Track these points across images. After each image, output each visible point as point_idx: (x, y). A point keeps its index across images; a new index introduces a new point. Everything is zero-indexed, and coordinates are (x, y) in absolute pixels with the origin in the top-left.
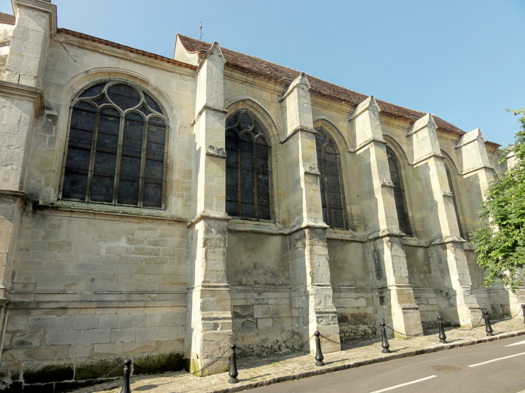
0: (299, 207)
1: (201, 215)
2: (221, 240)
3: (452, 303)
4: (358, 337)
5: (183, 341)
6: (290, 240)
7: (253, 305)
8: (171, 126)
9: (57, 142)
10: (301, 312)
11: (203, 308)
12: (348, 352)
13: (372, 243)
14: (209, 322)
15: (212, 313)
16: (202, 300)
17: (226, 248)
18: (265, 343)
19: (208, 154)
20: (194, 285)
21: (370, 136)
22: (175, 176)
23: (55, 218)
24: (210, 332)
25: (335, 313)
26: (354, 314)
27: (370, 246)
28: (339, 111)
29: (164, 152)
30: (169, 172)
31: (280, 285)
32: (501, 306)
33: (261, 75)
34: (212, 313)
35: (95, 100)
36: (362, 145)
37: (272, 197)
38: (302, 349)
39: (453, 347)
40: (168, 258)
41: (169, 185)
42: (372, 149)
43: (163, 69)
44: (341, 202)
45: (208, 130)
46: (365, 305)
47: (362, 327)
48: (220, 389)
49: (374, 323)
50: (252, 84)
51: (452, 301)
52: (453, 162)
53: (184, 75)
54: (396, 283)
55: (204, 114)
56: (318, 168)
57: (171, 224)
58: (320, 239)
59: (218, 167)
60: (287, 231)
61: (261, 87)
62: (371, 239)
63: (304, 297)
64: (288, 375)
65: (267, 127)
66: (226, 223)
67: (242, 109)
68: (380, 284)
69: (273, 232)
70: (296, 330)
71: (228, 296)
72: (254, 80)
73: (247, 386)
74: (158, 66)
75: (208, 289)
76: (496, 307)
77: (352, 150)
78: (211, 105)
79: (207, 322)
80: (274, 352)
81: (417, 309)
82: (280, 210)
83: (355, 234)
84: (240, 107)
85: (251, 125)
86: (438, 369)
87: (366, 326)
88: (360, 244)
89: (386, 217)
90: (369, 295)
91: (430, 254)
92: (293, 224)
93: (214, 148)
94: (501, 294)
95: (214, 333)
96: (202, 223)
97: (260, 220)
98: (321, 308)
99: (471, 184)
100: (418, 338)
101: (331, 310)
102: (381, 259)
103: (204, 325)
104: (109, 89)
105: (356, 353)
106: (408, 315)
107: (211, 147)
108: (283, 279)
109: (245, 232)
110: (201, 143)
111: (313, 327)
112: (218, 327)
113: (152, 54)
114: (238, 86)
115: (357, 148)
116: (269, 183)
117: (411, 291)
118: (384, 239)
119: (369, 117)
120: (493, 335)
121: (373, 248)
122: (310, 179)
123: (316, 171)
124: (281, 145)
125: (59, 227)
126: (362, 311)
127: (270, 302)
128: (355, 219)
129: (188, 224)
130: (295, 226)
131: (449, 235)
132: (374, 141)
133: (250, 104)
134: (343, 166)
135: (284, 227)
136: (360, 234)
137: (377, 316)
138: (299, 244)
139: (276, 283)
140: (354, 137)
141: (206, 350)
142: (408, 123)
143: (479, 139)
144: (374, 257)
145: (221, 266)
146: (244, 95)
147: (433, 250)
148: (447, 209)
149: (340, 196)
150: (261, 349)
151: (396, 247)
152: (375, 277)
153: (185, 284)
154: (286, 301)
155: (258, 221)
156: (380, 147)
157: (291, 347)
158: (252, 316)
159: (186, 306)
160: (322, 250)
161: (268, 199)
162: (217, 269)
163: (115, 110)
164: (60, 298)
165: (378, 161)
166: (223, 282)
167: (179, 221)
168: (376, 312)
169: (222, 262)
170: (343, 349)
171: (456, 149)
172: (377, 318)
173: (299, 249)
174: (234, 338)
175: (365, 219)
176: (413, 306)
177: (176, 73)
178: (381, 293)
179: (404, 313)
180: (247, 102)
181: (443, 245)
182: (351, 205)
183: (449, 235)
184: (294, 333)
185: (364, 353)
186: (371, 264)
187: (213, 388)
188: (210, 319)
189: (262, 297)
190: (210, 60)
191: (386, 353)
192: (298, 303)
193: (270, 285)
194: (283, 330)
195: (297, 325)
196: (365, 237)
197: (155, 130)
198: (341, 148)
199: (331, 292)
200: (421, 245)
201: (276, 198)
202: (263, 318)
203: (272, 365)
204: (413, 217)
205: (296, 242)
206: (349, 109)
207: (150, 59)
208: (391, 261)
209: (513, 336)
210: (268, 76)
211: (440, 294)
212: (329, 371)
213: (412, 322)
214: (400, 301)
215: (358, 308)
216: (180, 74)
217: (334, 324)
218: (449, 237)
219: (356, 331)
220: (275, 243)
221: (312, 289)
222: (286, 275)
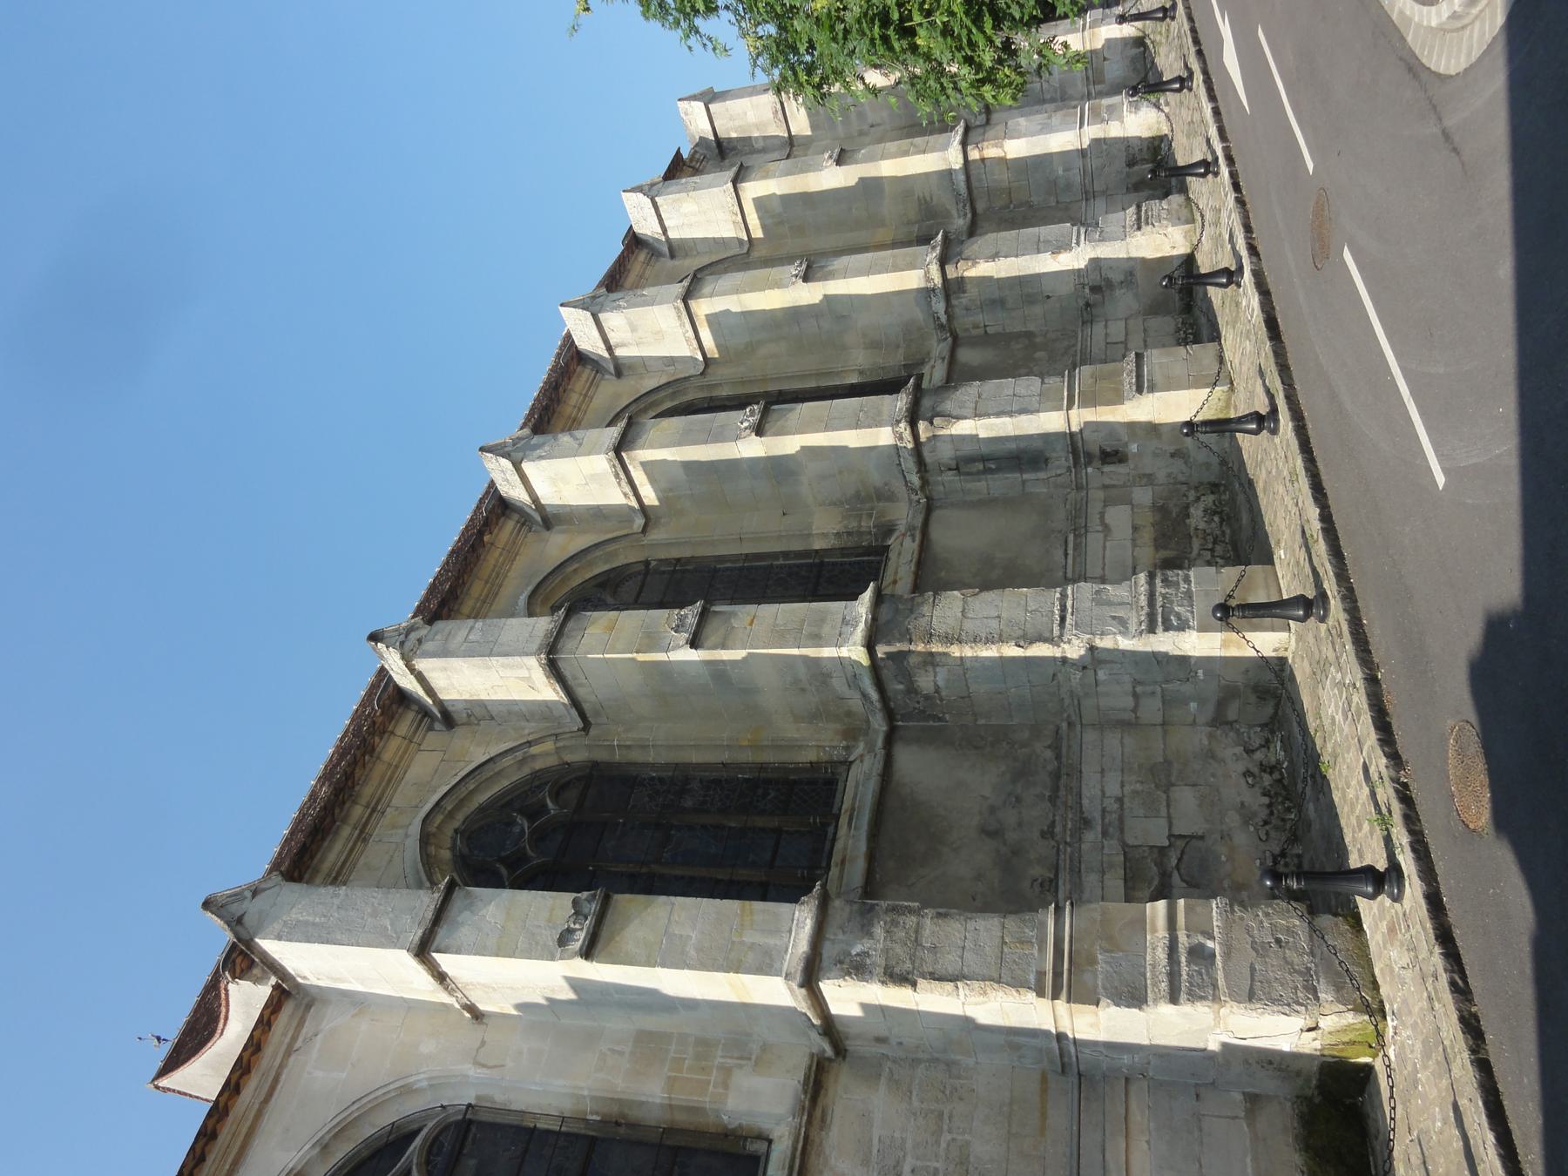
0: (802, 672)
1: (801, 986)
2: (895, 923)
3: (1122, 278)
4: (1228, 531)
5: (1254, 1101)
6: (907, 717)
7: (1124, 845)
8: (467, 1097)
10: (1149, 689)
11: (1133, 998)
12: (1278, 542)
13: (934, 478)
14: (1185, 977)
15: (1153, 966)
16: (1104, 1002)
17: (925, 905)
18: (1255, 814)
19: (588, 953)
20: (1047, 1033)
21: (601, 463)
22: (651, 1092)
24: (1220, 976)
25: (1151, 577)
26: (1155, 540)
27: (946, 482)
28: (511, 553)
29: (559, 1133)
30: (635, 1114)
31: (1058, 757)
32: (1131, 163)
33: (349, 776)
34: (1153, 966)
36: (628, 489)
37: (762, 767)
38: (1272, 686)
39: (1253, 250)
40: (946, 1137)
41: (682, 1119)
42: (639, 456)
43: (259, 1114)
44: (798, 566)
45: (504, 949)
46: (1128, 508)
47: (1197, 518)
48: (1429, 925)
49: (1184, 488)
50: (374, 810)
51: (1116, 277)
52: (711, 265)
53: (294, 1039)
54: (1060, 409)
55: (444, 961)
56: (682, 607)
57: (823, 1120)
58: (912, 611)
59: (636, 921)
60: (879, 724)
61: (393, 777)
62: (922, 478)
63: (1102, 675)
64: (1364, 698)
65: (526, 771)
66: (837, 903)
67: (453, 848)
68: (1061, 460)
69: (878, 766)
70: (1210, 709)
71: (1094, 910)
72: (364, 801)
73: (1411, 832)
74: (244, 1131)
75: (1069, 982)
76: (1134, 179)
77: (639, 522)
78: (416, 935)
79: (1184, 985)
80: (1285, 787)
81: (1139, 357)
82: (812, 744)
83: (902, 528)
84: (446, 854)
85: (512, 823)
86: (1322, 252)
87: (1192, 510)
88: (937, 514)
89: (857, 427)
90: (1097, 495)
91: (975, 332)
92: (856, 703)
93: (570, 931)
94: (1096, 163)
95: (1225, 963)
96: (827, 987)
97: (835, 811)
98: (1136, 619)
99: (781, 223)
100: (1228, 355)
101: (1143, 588)
102: (985, 450)
103: (1194, 997)
105: (1281, 513)
106: (1158, 378)
107: (564, 939)
108: (1038, 747)
109: (871, 857)
110: (547, 977)
111: (1200, 644)
112: (1202, 946)
113: (192, 1148)
114: (374, 853)
115: (634, 503)
116: (715, 775)
117: (1086, 370)
118: (923, 437)
119: (543, 462)
120: (1216, 159)
121: (949, 477)
122: (713, 631)
123: (691, 614)
124: (593, 732)
126: (1147, 518)
127: (1113, 789)
128: (855, 524)
129: (829, 1052)
130: (865, 696)
131: (921, 272)
132: (619, 449)
133: (439, 819)
134: (686, 553)
135: (867, 734)
136: (903, 513)
137: (1161, 476)
138: (925, 682)
139: (1050, 768)
140: (599, 514)
141: (1287, 994)
142: (579, 369)
143: (653, 193)
144: (979, 473)
145: (986, 929)
146: (407, 836)
147: (964, 322)
148: (846, 274)
149: (781, 567)
150: (1276, 828)
151: (948, 406)
152: (1042, 475)
153: (1044, 1079)
154: (1113, 740)
155: (837, 817)
156: (638, 436)
157: (1266, 734)
158: (1162, 851)
159: (1127, 1080)
160: (946, 609)
161: (768, 782)
162: (997, 941)
165: (679, 443)
166: (1043, 925)
167: (816, 1082)
168: (1149, 479)
169: (971, 925)
170: (1267, 558)
171: (672, 256)
172: (1169, 475)
173: (941, 683)
174: (1239, 895)
175: (857, 495)
176: (1132, 366)
177: (282, 1066)
178: (1090, 458)
179: (1152, 389)
180: (432, 829)
181: (952, 288)
182: (809, 535)
183: (921, 272)
184: (1219, 720)
185: (1281, 490)
186: (999, 484)
187: (1423, 954)
188: (1173, 976)
189: (1097, 815)
190: (259, 929)
191: (1277, 421)
192: (1118, 699)
193: (1056, 789)
194: (1210, 755)
195: (1193, 705)
196: (915, 498)
197: (472, 1162)
198: (627, 556)
199: (1086, 588)
200: (946, 354)
201: (769, 757)
202: (1169, 818)
203: (1330, 774)
204: (861, 372)
205: (916, 692)
206: (509, 526)
207: (210, 1158)
208: (993, 420)
209: (1217, 112)
210: (358, 753)
211: (1095, 311)
212: (1342, 576)
213: (1179, 369)
214: (1117, 399)
215: (1135, 529)
216: (289, 1052)
217: (1187, 580)
218: (927, 272)
219: (1210, 539)
220: (914, 764)
221: (1075, 642)
222: (1026, 734)
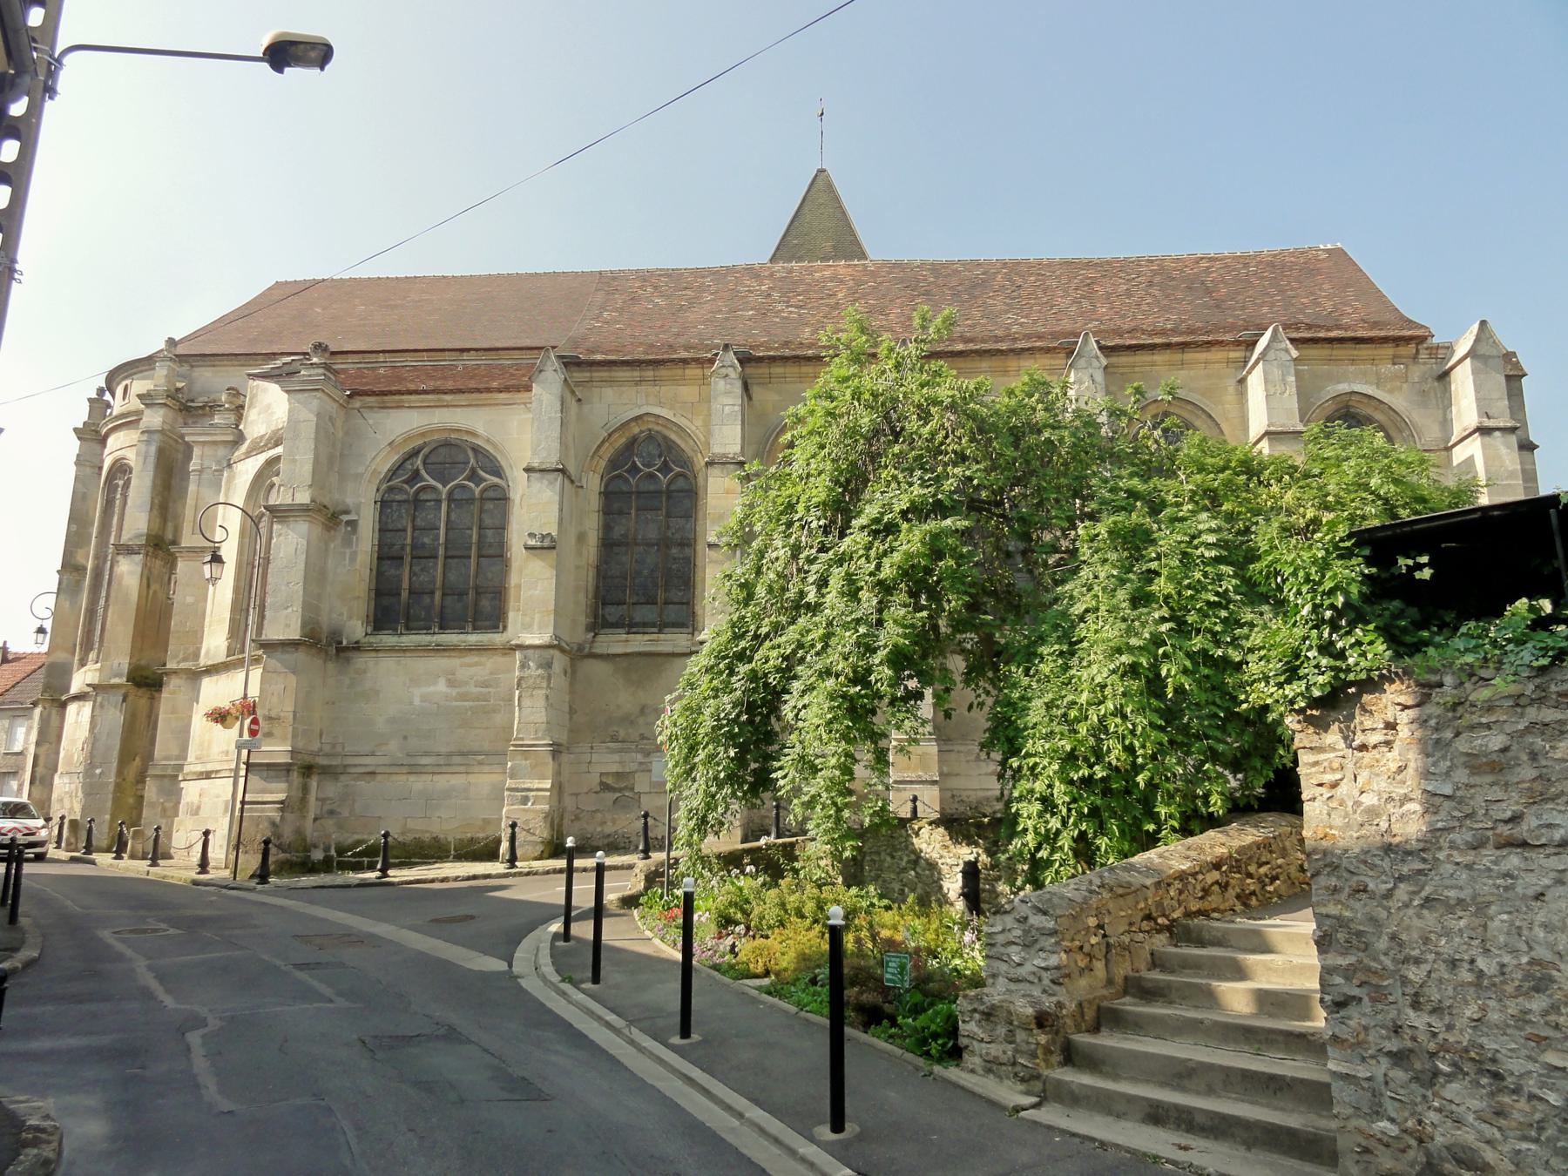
9: (359, 558)
23: (361, 661)
35: (406, 481)
65: (690, 453)
104: (426, 457)
125: (365, 671)
163: (433, 488)
164: (367, 760)
